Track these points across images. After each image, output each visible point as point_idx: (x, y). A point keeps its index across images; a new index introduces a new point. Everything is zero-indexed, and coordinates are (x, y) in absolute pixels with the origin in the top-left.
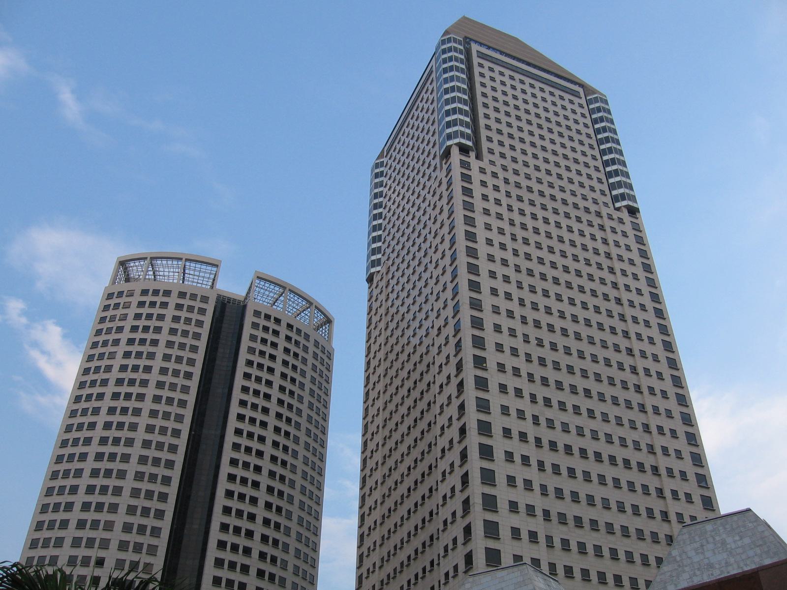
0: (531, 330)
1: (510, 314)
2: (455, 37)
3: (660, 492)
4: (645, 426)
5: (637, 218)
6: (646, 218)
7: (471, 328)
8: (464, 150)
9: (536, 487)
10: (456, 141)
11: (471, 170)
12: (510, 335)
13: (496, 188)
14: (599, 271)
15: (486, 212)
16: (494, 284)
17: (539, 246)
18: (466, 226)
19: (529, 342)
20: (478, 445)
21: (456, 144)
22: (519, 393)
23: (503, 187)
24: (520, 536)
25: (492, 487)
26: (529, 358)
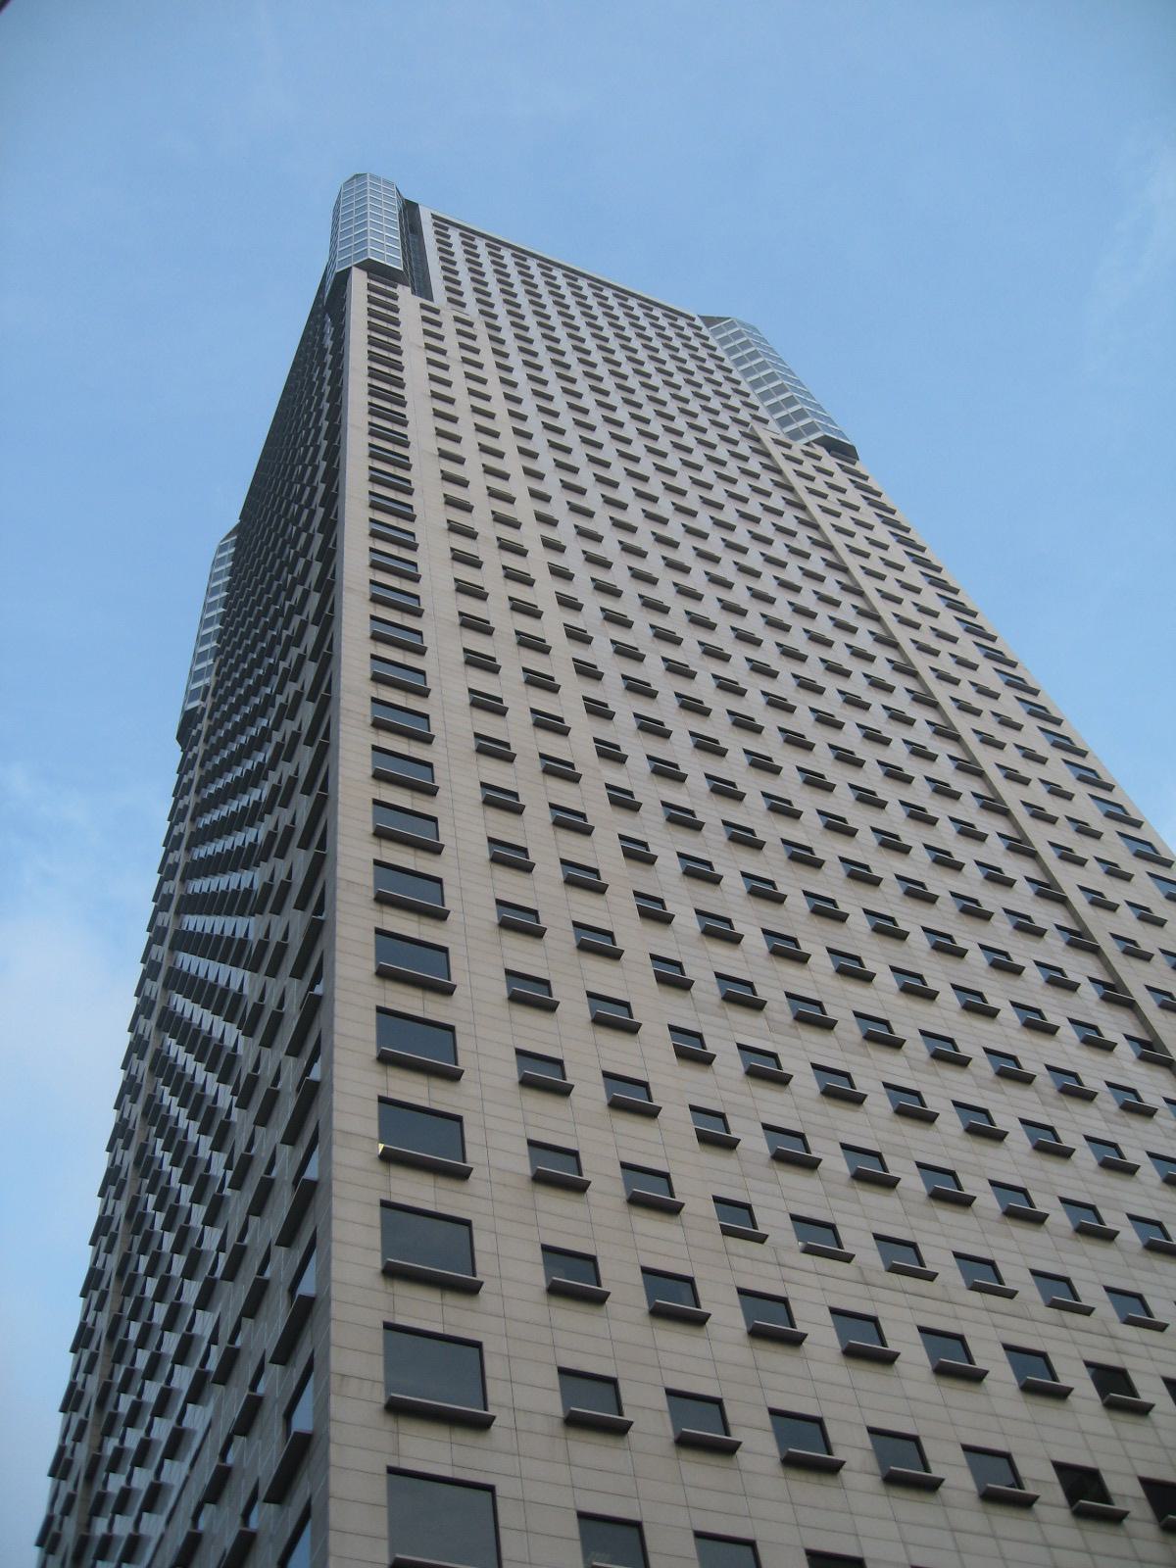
7: (379, 1283)
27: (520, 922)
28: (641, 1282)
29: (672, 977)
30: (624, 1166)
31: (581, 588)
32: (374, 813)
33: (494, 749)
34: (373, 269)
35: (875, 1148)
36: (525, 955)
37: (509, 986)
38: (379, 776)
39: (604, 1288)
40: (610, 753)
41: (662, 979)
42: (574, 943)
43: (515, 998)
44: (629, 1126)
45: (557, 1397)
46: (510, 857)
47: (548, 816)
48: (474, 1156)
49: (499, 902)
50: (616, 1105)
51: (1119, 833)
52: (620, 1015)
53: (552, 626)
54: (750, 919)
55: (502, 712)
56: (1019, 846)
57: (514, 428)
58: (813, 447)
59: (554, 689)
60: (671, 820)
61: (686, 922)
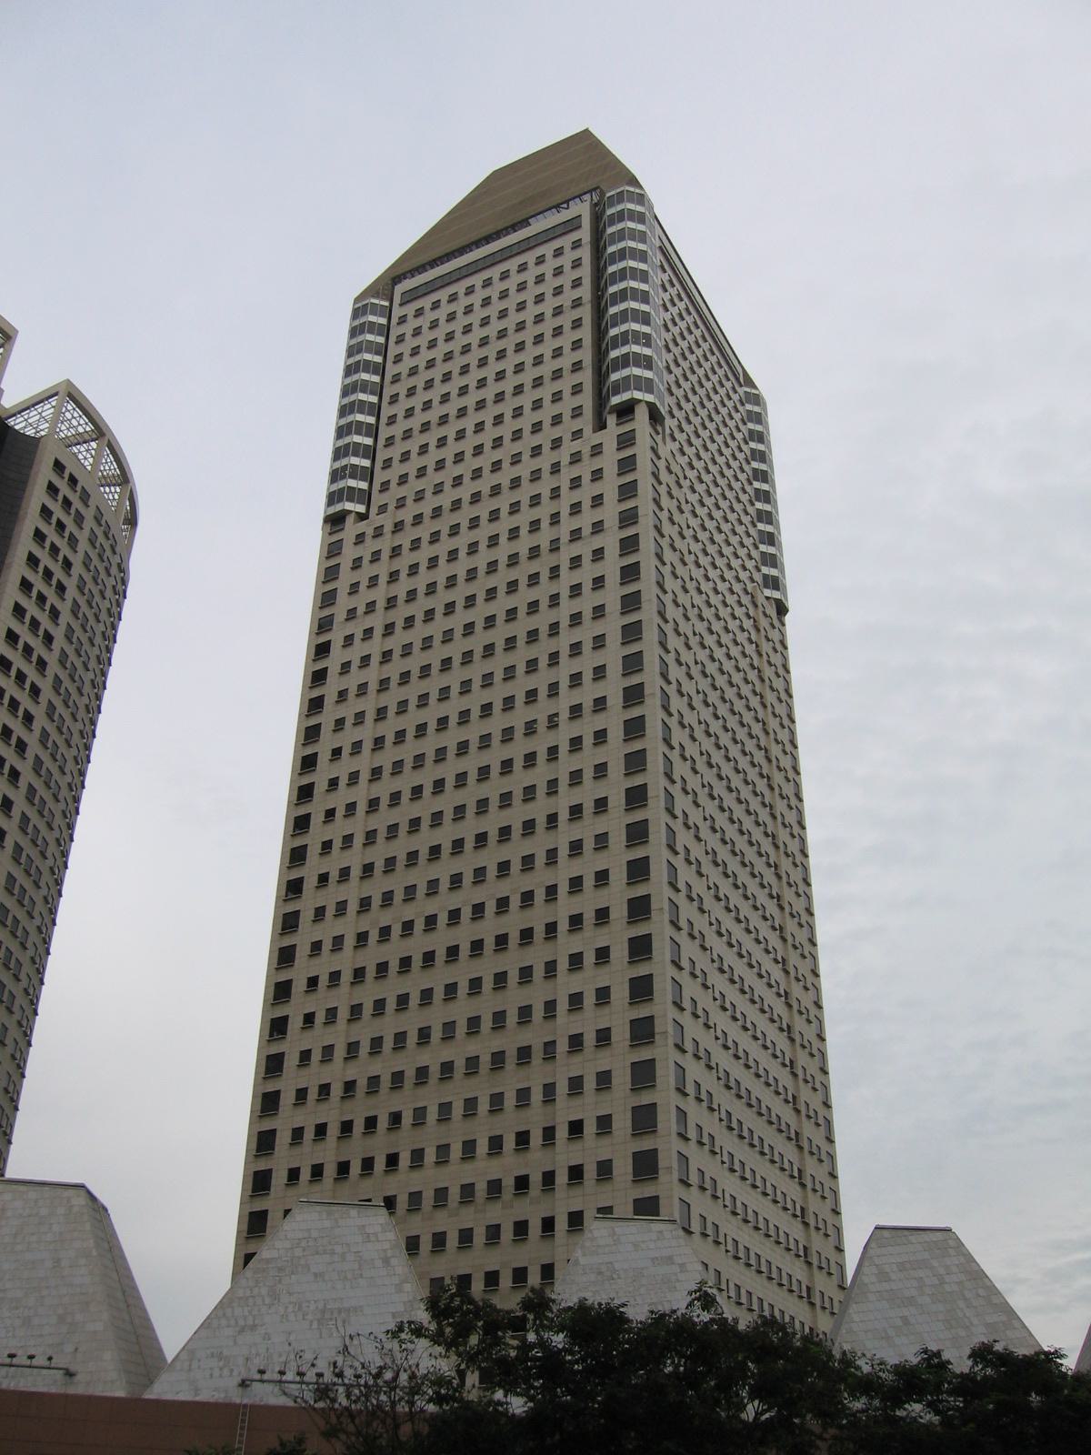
8: (655, 416)
10: (650, 398)
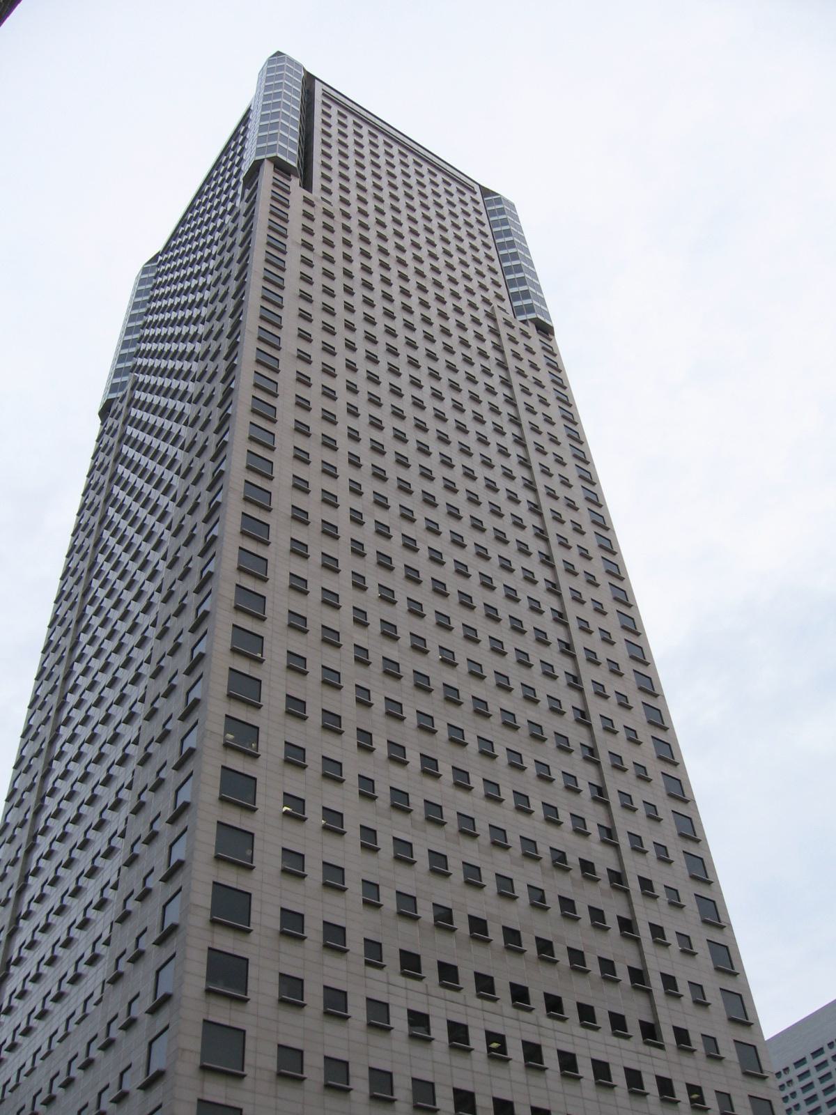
0: (374, 679)
1: (333, 772)
2: (284, 122)
3: (627, 926)
4: (604, 832)
5: (550, 340)
6: (561, 340)
7: (229, 653)
8: (280, 166)
9: (355, 944)
11: (261, 661)
12: (325, 828)
13: (331, 565)
14: (547, 682)
15: (300, 516)
16: (297, 733)
17: (419, 646)
18: (255, 415)
19: (371, 750)
20: (206, 954)
21: (269, 159)
22: (334, 822)
23: (347, 563)
24: (302, 1073)
25: (235, 1006)
26: (367, 790)
27: (303, 404)
28: (322, 995)
29: (355, 462)
30: (323, 626)
31: (355, 268)
32: (250, 429)
33: (306, 297)
34: (280, 166)
35: (414, 538)
36: (302, 471)
37: (290, 581)
38: (254, 411)
39: (307, 670)
40: (349, 308)
41: (352, 490)
42: (321, 530)
43: (293, 551)
44: (328, 575)
45: (275, 1061)
46: (305, 336)
47: (320, 390)
48: (268, 613)
49: (296, 421)
50: (324, 566)
51: (610, 584)
52: (333, 500)
53: (337, 252)
54: (392, 446)
55: (310, 341)
56: (520, 441)
57: (338, 112)
58: (528, 325)
59: (333, 246)
60: (369, 378)
61: (368, 496)
